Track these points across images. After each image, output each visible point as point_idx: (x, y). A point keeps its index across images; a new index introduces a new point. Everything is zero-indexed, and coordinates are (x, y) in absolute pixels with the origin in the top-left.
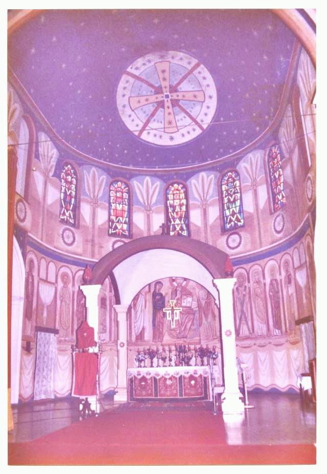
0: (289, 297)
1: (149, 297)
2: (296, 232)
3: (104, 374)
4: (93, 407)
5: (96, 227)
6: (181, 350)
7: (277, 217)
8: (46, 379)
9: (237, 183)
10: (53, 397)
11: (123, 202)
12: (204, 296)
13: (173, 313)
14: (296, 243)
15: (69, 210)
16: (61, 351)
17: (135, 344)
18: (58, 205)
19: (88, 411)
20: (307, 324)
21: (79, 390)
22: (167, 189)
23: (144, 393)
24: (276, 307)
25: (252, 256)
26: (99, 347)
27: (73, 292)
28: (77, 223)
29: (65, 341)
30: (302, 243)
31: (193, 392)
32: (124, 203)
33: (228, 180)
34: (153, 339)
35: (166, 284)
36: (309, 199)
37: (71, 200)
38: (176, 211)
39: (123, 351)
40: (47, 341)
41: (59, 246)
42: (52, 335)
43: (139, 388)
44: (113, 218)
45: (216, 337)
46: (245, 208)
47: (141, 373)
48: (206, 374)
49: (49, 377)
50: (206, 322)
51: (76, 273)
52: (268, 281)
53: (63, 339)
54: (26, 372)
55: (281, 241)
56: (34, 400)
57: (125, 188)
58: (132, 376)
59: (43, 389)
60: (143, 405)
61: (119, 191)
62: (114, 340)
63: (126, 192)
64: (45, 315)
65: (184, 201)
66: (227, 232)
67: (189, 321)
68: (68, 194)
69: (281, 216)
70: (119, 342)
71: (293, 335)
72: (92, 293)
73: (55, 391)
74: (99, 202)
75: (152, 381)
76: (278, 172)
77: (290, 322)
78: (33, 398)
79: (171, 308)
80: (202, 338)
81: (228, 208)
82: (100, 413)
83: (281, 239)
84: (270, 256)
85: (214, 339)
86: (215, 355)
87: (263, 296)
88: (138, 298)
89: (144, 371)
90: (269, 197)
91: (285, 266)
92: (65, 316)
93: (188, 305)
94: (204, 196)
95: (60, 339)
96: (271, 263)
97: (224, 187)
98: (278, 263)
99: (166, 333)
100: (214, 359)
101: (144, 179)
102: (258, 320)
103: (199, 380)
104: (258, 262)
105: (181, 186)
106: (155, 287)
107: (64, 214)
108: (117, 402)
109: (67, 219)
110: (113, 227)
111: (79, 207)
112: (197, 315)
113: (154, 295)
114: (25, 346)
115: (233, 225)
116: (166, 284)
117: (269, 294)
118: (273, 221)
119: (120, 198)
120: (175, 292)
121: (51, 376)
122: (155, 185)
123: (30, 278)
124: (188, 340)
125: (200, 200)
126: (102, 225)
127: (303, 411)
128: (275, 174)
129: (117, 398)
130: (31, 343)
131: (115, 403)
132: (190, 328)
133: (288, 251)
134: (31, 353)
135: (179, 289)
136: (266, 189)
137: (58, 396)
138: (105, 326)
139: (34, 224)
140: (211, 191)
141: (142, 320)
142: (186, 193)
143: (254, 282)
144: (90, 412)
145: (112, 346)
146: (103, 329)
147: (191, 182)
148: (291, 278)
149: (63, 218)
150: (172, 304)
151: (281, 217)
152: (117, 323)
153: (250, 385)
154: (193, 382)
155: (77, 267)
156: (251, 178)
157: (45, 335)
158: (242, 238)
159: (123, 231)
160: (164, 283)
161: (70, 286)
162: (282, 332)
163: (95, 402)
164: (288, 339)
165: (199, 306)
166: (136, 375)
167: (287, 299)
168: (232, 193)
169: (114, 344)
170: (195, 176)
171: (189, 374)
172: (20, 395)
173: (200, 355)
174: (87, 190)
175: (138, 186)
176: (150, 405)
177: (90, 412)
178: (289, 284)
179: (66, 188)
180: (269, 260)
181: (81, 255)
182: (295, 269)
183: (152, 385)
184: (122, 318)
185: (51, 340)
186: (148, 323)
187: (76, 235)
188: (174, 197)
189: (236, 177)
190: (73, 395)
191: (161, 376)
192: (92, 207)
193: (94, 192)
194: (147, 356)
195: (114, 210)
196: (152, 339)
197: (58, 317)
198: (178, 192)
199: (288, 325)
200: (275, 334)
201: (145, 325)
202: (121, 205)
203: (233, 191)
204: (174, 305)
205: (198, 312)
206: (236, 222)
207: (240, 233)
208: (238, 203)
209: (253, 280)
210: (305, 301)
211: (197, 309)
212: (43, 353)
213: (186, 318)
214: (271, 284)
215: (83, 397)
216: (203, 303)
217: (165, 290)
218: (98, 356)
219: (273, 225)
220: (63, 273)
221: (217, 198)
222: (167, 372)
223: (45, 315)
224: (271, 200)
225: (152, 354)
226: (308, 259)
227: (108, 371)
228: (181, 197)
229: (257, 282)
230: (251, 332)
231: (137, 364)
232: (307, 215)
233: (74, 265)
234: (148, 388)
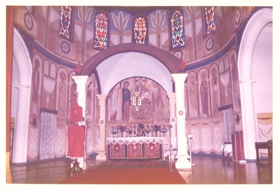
0: (215, 92)
1: (120, 91)
2: (222, 49)
3: (89, 142)
4: (81, 166)
5: (85, 42)
6: (141, 126)
7: (208, 39)
8: (48, 145)
9: (182, 17)
10: (53, 157)
11: (104, 27)
12: (156, 92)
13: (137, 101)
14: (223, 56)
15: (66, 29)
16: (59, 126)
17: (110, 123)
18: (58, 24)
19: (77, 168)
20: (228, 110)
21: (71, 153)
22: (134, 20)
23: (117, 155)
24: (205, 99)
27: (69, 86)
28: (71, 38)
29: (62, 119)
30: (227, 56)
32: (105, 27)
33: (175, 16)
34: (122, 120)
35: (131, 82)
37: (68, 22)
38: (140, 35)
39: (102, 126)
40: (49, 119)
41: (60, 54)
42: (53, 115)
43: (114, 151)
44: (97, 37)
45: (164, 119)
46: (186, 34)
47: (116, 141)
48: (161, 142)
49: (51, 143)
50: (157, 109)
51: (70, 73)
52: (200, 82)
53: (61, 117)
56: (40, 159)
57: (105, 18)
58: (110, 143)
59: (47, 152)
60: (117, 164)
61: (101, 20)
62: (96, 120)
63: (106, 21)
64: (48, 100)
65: (145, 29)
66: (173, 50)
67: (146, 108)
68: (66, 17)
70: (100, 120)
71: (216, 117)
73: (55, 153)
74: (88, 25)
76: (210, 9)
77: (214, 109)
79: (136, 98)
80: (154, 119)
81: (175, 34)
82: (86, 170)
83: (210, 54)
85: (163, 120)
86: (165, 130)
87: (196, 92)
88: (113, 92)
89: (118, 140)
90: (203, 27)
91: (202, 76)
93: (146, 97)
94: (158, 26)
95: (58, 117)
96: (203, 70)
97: (172, 20)
98: (207, 71)
99: (131, 116)
101: (119, 12)
102: (192, 108)
103: (121, 147)
106: (124, 85)
107: (62, 31)
109: (65, 34)
110: (97, 44)
111: (74, 27)
112: (152, 104)
113: (124, 90)
114: (32, 121)
115: (177, 46)
116: (131, 82)
118: (205, 43)
119: (101, 24)
120: (137, 89)
121: (52, 143)
122: (126, 17)
123: (36, 72)
124: (145, 121)
125: (156, 29)
126: (90, 41)
127: (224, 167)
128: (208, 11)
129: (98, 158)
130: (37, 120)
131: (96, 161)
132: (147, 113)
133: (215, 62)
134: (37, 127)
135: (140, 87)
137: (57, 156)
138: (90, 110)
140: (164, 22)
141: (115, 107)
143: (190, 83)
144: (79, 169)
145: (95, 123)
146: (89, 112)
147: (150, 17)
148: (216, 81)
149: (62, 33)
150: (137, 95)
151: (211, 39)
152: (98, 107)
153: (196, 148)
154: (152, 148)
155: (71, 69)
156: (191, 14)
157: (47, 114)
158: (183, 54)
159: (104, 46)
160: (130, 82)
161: (66, 81)
162: (208, 116)
163: (83, 162)
166: (112, 142)
167: (213, 93)
168: (178, 24)
170: (153, 13)
171: (150, 142)
172: (28, 157)
173: (155, 130)
174: (79, 16)
175: (115, 17)
176: (122, 164)
177: (79, 169)
179: (64, 13)
180: (201, 69)
181: (74, 61)
182: (221, 74)
183: (123, 150)
184: (102, 104)
185: (52, 118)
187: (71, 47)
188: (138, 26)
189: (180, 13)
191: (129, 143)
194: (119, 130)
195: (98, 32)
196: (121, 119)
197: (57, 102)
198: (141, 23)
199: (212, 111)
200: (203, 117)
201: (117, 110)
202: (103, 29)
203: (178, 23)
204: (138, 96)
205: (152, 102)
206: (179, 43)
207: (182, 51)
208: (181, 31)
209: (189, 82)
210: (226, 95)
211: (152, 100)
212: (46, 127)
213: (144, 106)
214: (202, 84)
215: (74, 158)
216: (156, 96)
217: (131, 87)
218: (85, 128)
219: (205, 45)
220: (61, 72)
221: (168, 27)
222: (134, 140)
223: (48, 100)
224: (205, 29)
225: (122, 129)
226: (231, 66)
227: (92, 140)
228: (143, 26)
230: (187, 115)
232: (234, 35)
233: (69, 67)
234: (120, 151)
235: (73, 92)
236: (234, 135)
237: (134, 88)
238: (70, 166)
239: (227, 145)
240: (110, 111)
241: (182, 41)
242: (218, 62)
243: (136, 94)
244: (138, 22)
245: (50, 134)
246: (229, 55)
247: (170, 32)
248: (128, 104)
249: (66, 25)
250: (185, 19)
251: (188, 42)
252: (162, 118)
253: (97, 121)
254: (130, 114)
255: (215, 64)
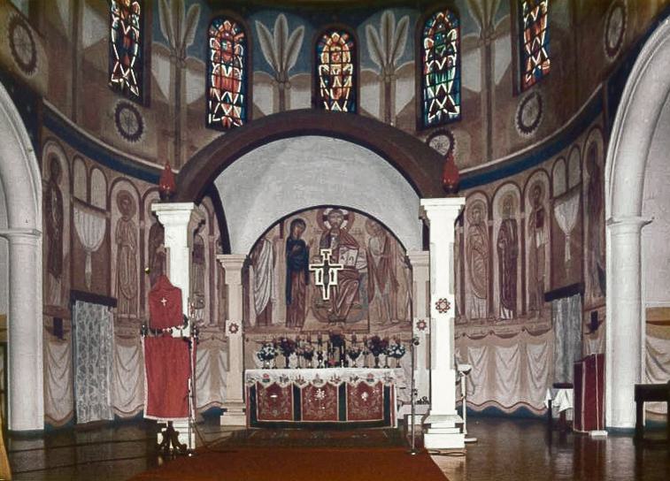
0: (536, 251)
1: (281, 246)
3: (203, 378)
4: (183, 439)
7: (527, 99)
8: (97, 386)
11: (233, 62)
13: (326, 273)
16: (123, 338)
17: (256, 330)
21: (157, 405)
22: (319, 41)
23: (275, 413)
25: (470, 176)
26: (192, 328)
28: (144, 94)
29: (130, 319)
30: (578, 147)
31: (364, 413)
32: (237, 63)
33: (435, 28)
35: (311, 221)
36: (608, 48)
38: (334, 86)
39: (235, 339)
42: (104, 308)
43: (266, 404)
44: (215, 92)
45: (396, 321)
47: (271, 378)
48: (389, 381)
49: (103, 383)
50: (380, 294)
51: (145, 195)
52: (498, 221)
54: (56, 373)
55: (530, 148)
56: (78, 422)
57: (238, 33)
63: (240, 43)
64: (89, 269)
65: (350, 68)
66: (427, 131)
69: (536, 96)
70: (228, 323)
72: (177, 220)
73: (115, 408)
75: (290, 392)
77: (533, 297)
78: (75, 418)
79: (323, 264)
81: (433, 84)
83: (530, 142)
84: (507, 176)
85: (394, 324)
86: (401, 351)
87: (485, 249)
88: (261, 249)
89: (275, 374)
92: (127, 275)
99: (310, 313)
100: (398, 357)
104: (482, 187)
105: (345, 36)
106: (292, 229)
107: (119, 74)
108: (225, 429)
111: (149, 61)
113: (291, 243)
114: (52, 325)
116: (311, 221)
117: (498, 245)
119: (227, 52)
120: (326, 242)
121: (106, 382)
123: (54, 193)
126: (195, 104)
129: (226, 420)
132: (352, 304)
133: (543, 165)
135: (335, 235)
136: (510, 43)
139: (54, 79)
142: (354, 51)
143: (471, 225)
146: (199, 301)
148: (543, 219)
149: (116, 81)
150: (326, 257)
151: (535, 99)
153: (479, 399)
154: (365, 395)
157: (90, 306)
159: (235, 120)
161: (136, 218)
164: (527, 326)
165: (370, 266)
166: (261, 382)
168: (442, 54)
169: (217, 329)
171: (359, 381)
172: (47, 416)
173: (372, 350)
175: (264, 31)
178: (538, 227)
179: (121, 19)
180: (504, 184)
181: (155, 162)
183: (290, 400)
184: (233, 280)
186: (277, 293)
188: (330, 58)
189: (451, 20)
190: (145, 416)
191: (307, 384)
192: (174, 67)
193: (177, 37)
195: (216, 76)
197: (114, 275)
199: (528, 302)
200: (503, 317)
202: (230, 69)
206: (445, 111)
207: (452, 132)
210: (568, 257)
211: (366, 270)
215: (165, 421)
216: (377, 259)
218: (190, 343)
220: (121, 192)
221: (413, 62)
222: (317, 375)
223: (89, 269)
225: (287, 347)
226: (586, 175)
227: (208, 374)
228: (344, 60)
229: (476, 225)
231: (260, 363)
232: (600, 86)
233: (141, 178)
235: (156, 248)
236: (582, 365)
237: (319, 237)
238: (156, 439)
239: (561, 392)
240: (255, 300)
241: (454, 104)
242: (551, 167)
243: (324, 255)
244: (330, 47)
245: (100, 358)
246: (582, 145)
247: (419, 77)
248: (303, 282)
249: (127, 56)
250: (463, 38)
251: (471, 105)
252: (391, 320)
253: (222, 325)
254: (306, 309)
255: (543, 170)
